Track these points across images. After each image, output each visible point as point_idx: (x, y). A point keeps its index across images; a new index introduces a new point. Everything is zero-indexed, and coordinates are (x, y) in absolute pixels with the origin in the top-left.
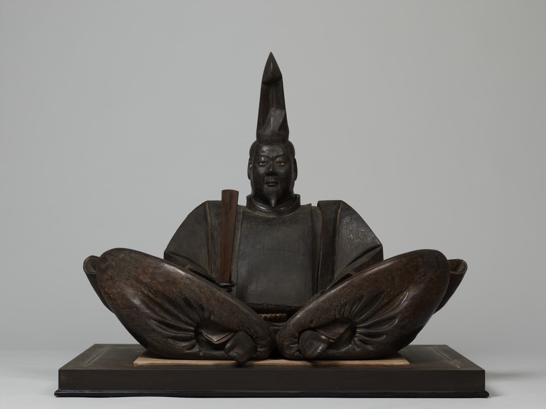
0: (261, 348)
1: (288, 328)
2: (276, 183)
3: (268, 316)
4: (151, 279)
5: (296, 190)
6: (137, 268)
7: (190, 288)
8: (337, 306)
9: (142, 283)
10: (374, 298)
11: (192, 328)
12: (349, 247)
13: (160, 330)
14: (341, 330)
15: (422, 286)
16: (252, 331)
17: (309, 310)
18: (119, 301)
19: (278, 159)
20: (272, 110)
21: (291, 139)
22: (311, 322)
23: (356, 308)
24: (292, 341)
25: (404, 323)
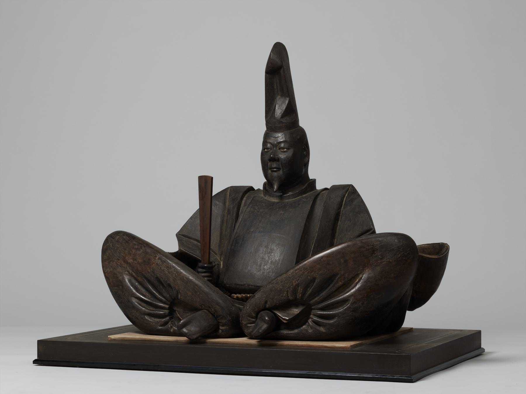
0: (223, 326)
2: (278, 169)
6: (125, 249)
8: (289, 288)
10: (329, 280)
11: (167, 306)
14: (296, 311)
15: (378, 269)
19: (282, 145)
20: (278, 98)
21: (301, 124)
22: (266, 302)
23: (310, 291)
24: (250, 320)
25: (356, 305)
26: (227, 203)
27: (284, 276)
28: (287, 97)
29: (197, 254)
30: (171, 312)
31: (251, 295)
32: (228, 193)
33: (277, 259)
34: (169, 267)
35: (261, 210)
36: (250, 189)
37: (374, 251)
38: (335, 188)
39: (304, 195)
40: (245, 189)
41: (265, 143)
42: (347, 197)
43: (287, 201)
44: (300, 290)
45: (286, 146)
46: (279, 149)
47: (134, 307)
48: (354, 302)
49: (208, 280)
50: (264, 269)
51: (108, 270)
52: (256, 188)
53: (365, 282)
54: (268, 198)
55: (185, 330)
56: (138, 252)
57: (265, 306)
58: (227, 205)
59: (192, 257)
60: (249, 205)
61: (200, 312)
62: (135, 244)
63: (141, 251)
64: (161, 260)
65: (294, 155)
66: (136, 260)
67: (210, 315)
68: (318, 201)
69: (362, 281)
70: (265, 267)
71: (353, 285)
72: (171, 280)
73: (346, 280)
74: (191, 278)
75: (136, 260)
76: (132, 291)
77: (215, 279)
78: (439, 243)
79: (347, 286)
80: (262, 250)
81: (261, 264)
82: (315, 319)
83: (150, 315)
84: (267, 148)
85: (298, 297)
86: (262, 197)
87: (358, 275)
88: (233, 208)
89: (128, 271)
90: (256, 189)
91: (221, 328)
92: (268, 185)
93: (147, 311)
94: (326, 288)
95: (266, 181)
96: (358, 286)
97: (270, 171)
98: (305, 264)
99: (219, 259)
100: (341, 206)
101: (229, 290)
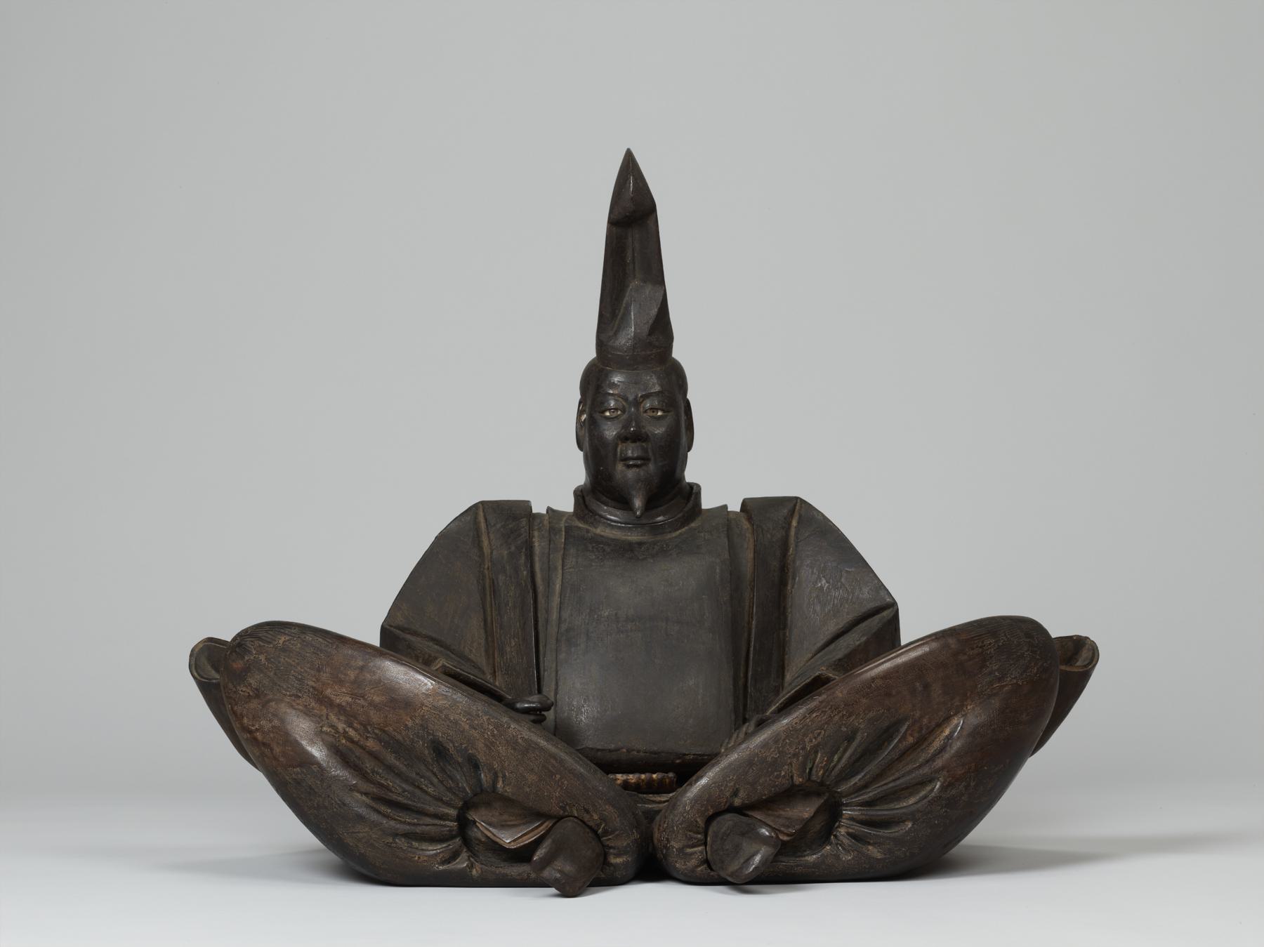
0: (618, 855)
1: (681, 809)
3: (632, 778)
4: (353, 695)
5: (691, 474)
6: (319, 670)
7: (447, 716)
8: (795, 755)
9: (330, 704)
12: (818, 608)
13: (374, 817)
15: (996, 703)
16: (596, 817)
17: (730, 764)
18: (277, 750)
22: (735, 794)
25: (954, 792)
42: (785, 531)
48: (950, 784)
52: (539, 508)
58: (486, 550)
72: (480, 745)
78: (1071, 637)
89: (332, 726)
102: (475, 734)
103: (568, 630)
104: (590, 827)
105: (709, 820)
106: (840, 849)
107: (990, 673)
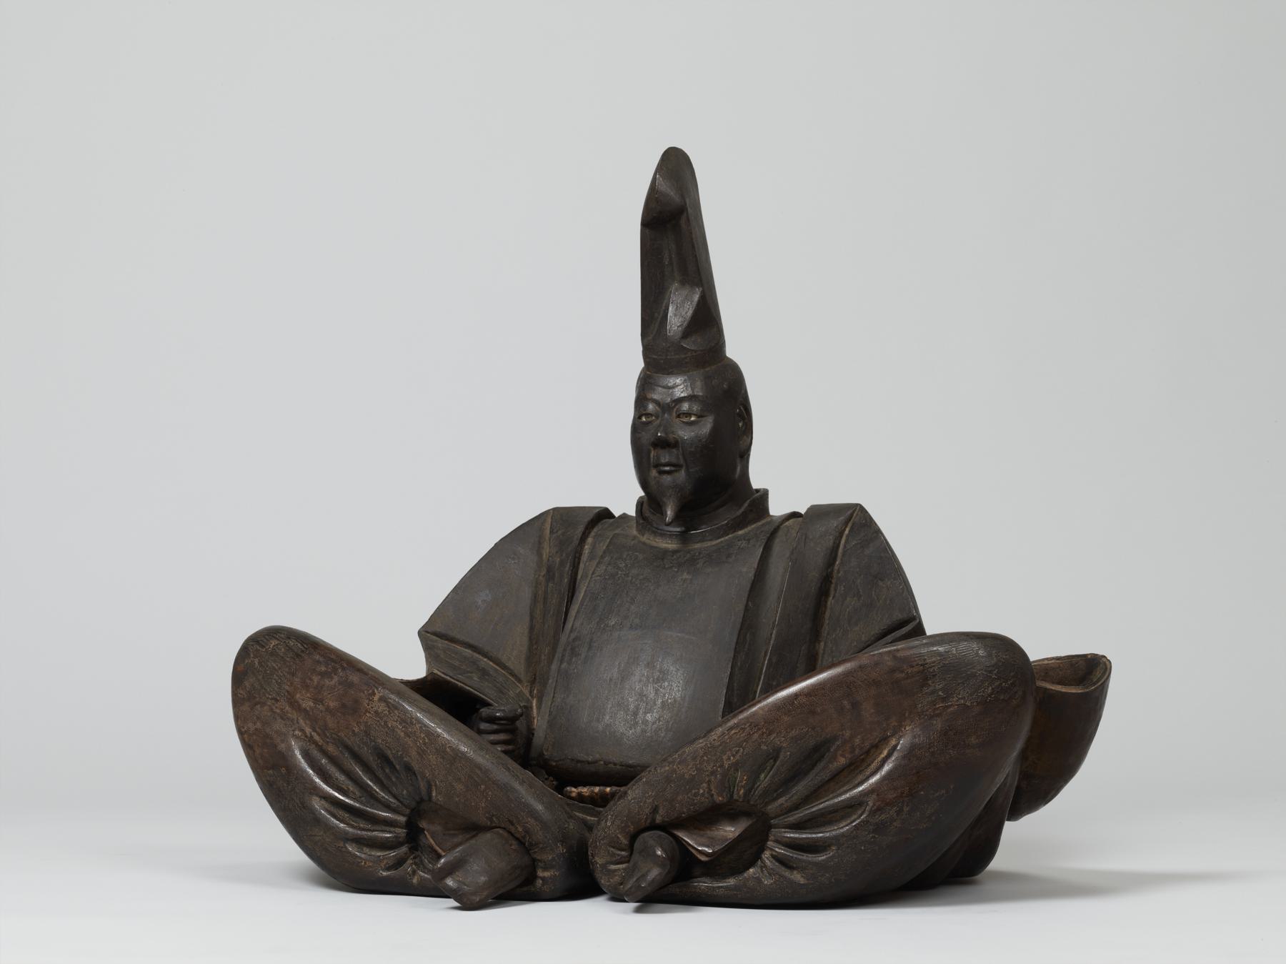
0: (545, 869)
2: (677, 466)
3: (585, 790)
5: (757, 479)
6: (293, 674)
8: (713, 773)
10: (816, 753)
14: (730, 831)
15: (938, 724)
21: (731, 352)
22: (655, 810)
23: (765, 780)
25: (883, 817)
26: (546, 551)
27: (701, 743)
28: (697, 286)
29: (471, 683)
30: (413, 835)
31: (615, 788)
32: (548, 526)
33: (678, 695)
34: (407, 721)
35: (634, 571)
36: (604, 515)
37: (926, 679)
38: (818, 513)
39: (740, 532)
40: (591, 516)
41: (641, 401)
43: (698, 546)
44: (741, 778)
45: (695, 408)
46: (678, 416)
47: (318, 821)
48: (879, 809)
49: (505, 752)
50: (645, 722)
51: (251, 726)
53: (904, 757)
54: (648, 539)
55: (450, 882)
56: (327, 682)
57: (654, 820)
59: (461, 690)
60: (602, 557)
61: (488, 835)
62: (319, 662)
63: (336, 679)
64: (388, 704)
65: (715, 430)
66: (321, 701)
67: (514, 842)
68: (777, 546)
69: (896, 755)
70: (649, 717)
71: (874, 766)
72: (414, 753)
73: (857, 752)
74: (464, 749)
75: (321, 701)
76: (313, 781)
77: (524, 753)
79: (857, 767)
80: (639, 672)
81: (637, 708)
82: (780, 850)
83: (359, 841)
84: (648, 415)
85: (735, 797)
86: (635, 537)
87: (885, 740)
88: (562, 563)
89: (302, 730)
90: (617, 515)
91: (540, 873)
92: (650, 504)
93: (351, 830)
94: (807, 773)
95: (643, 494)
96: (887, 768)
97: (654, 473)
98: (754, 714)
99: (526, 692)
100: (835, 559)
101: (561, 776)
102: (409, 741)
103: (574, 640)
104: (517, 839)
105: (633, 838)
106: (758, 875)
107: (933, 693)
